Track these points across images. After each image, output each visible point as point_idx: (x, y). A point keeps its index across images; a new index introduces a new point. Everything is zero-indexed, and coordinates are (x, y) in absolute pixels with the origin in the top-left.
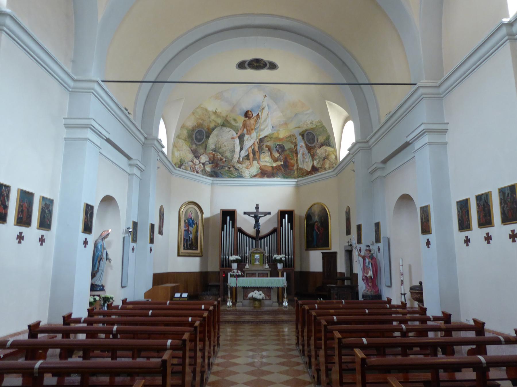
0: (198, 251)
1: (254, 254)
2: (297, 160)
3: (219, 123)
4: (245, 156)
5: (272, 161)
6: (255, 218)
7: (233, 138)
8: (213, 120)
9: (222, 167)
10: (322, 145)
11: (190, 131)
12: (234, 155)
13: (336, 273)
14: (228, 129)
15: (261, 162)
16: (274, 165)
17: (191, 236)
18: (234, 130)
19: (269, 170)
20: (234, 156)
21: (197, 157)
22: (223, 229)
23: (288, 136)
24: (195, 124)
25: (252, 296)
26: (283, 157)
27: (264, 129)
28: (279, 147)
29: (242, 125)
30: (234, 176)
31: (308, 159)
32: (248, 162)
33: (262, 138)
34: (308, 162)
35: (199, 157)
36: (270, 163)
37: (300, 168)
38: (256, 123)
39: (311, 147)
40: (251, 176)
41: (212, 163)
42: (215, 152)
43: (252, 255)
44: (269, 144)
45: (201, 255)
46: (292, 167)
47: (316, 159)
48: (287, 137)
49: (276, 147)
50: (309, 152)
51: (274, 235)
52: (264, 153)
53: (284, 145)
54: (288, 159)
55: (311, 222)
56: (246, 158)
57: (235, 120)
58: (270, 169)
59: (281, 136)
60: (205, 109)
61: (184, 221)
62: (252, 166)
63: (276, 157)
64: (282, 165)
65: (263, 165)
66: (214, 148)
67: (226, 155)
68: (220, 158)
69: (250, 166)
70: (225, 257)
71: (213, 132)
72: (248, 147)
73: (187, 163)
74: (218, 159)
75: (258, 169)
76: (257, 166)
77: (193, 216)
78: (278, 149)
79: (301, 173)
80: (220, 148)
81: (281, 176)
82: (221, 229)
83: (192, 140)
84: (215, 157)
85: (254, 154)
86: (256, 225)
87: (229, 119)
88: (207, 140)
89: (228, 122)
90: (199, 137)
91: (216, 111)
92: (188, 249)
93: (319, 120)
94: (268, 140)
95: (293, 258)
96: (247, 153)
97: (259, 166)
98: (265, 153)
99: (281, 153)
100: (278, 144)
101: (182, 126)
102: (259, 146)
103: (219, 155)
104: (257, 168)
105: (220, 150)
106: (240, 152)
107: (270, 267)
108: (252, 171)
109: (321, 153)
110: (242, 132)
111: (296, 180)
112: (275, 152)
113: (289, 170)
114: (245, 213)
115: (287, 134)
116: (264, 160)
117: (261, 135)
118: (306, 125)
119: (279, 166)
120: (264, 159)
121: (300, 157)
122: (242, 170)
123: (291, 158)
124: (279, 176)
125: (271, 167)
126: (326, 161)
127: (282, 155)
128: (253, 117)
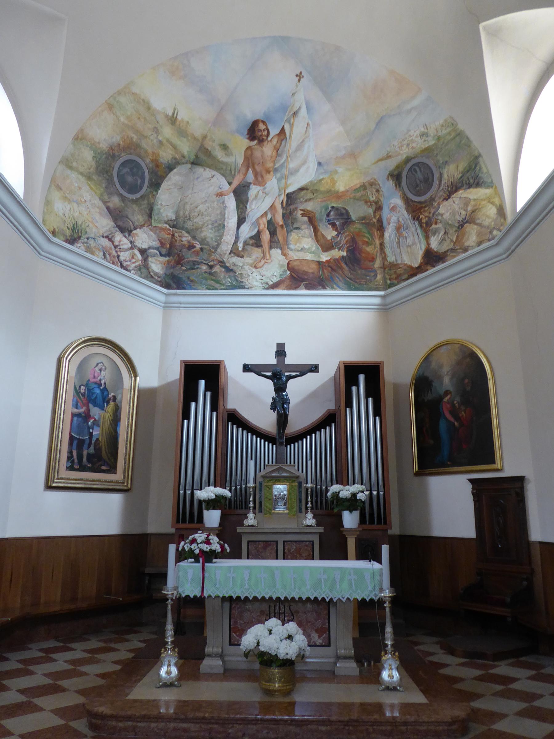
0: (118, 476)
1: (270, 483)
2: (382, 245)
3: (186, 153)
4: (251, 238)
5: (318, 248)
6: (273, 381)
7: (220, 194)
8: (168, 141)
9: (194, 265)
10: (454, 189)
11: (104, 156)
12: (221, 236)
13: (529, 544)
14: (208, 173)
15: (292, 250)
16: (324, 257)
17: (96, 432)
18: (223, 175)
19: (311, 271)
20: (224, 238)
21: (126, 230)
22: (186, 415)
23: (358, 186)
24: (117, 139)
25: (258, 643)
26: (345, 238)
27: (295, 171)
28: (336, 215)
29: (242, 161)
30: (222, 287)
31: (412, 238)
32: (257, 253)
33: (294, 192)
34: (414, 243)
35: (130, 232)
36: (313, 253)
37: (390, 263)
38: (277, 155)
39: (420, 203)
40: (267, 286)
41: (168, 255)
42: (175, 229)
43: (264, 484)
44: (309, 206)
45: (125, 488)
46: (369, 264)
47: (435, 232)
48: (356, 189)
49: (328, 215)
50: (416, 218)
51: (329, 433)
52: (297, 228)
53: (347, 208)
54: (360, 243)
55: (429, 397)
56: (252, 242)
57: (224, 147)
58: (312, 269)
59: (341, 187)
60: (143, 100)
61: (75, 387)
62: (269, 261)
63: (329, 238)
64: (343, 256)
65: (295, 258)
66: (174, 218)
67: (203, 235)
68: (189, 242)
69: (263, 262)
70: (188, 492)
71: (169, 175)
72: (259, 214)
73: (94, 239)
74: (184, 245)
75: (282, 270)
76: (280, 261)
77: (106, 377)
78: (334, 219)
79: (394, 276)
80: (189, 219)
81: (341, 284)
82: (181, 411)
83: (110, 181)
84: (176, 241)
85: (273, 233)
86: (278, 399)
87: (209, 145)
88: (155, 193)
89: (208, 153)
90: (130, 179)
91: (173, 114)
92: (82, 468)
93: (445, 121)
94: (308, 197)
95: (384, 494)
96: (256, 230)
97: (287, 263)
98: (302, 230)
99: (341, 230)
100: (333, 207)
101: (77, 135)
102: (285, 211)
103: (186, 235)
104: (281, 266)
105: (189, 225)
106: (238, 228)
107: (318, 524)
108: (268, 274)
109: (451, 211)
110: (243, 179)
111: (382, 293)
112: (327, 227)
113: (364, 272)
114: (247, 368)
115: (356, 182)
116: (298, 246)
117: (290, 184)
118: (408, 145)
119: (337, 261)
120: (298, 245)
121: (389, 237)
122: (243, 272)
123: (366, 239)
124: (338, 286)
125: (317, 263)
126: (468, 229)
127: (343, 233)
128: (269, 139)
